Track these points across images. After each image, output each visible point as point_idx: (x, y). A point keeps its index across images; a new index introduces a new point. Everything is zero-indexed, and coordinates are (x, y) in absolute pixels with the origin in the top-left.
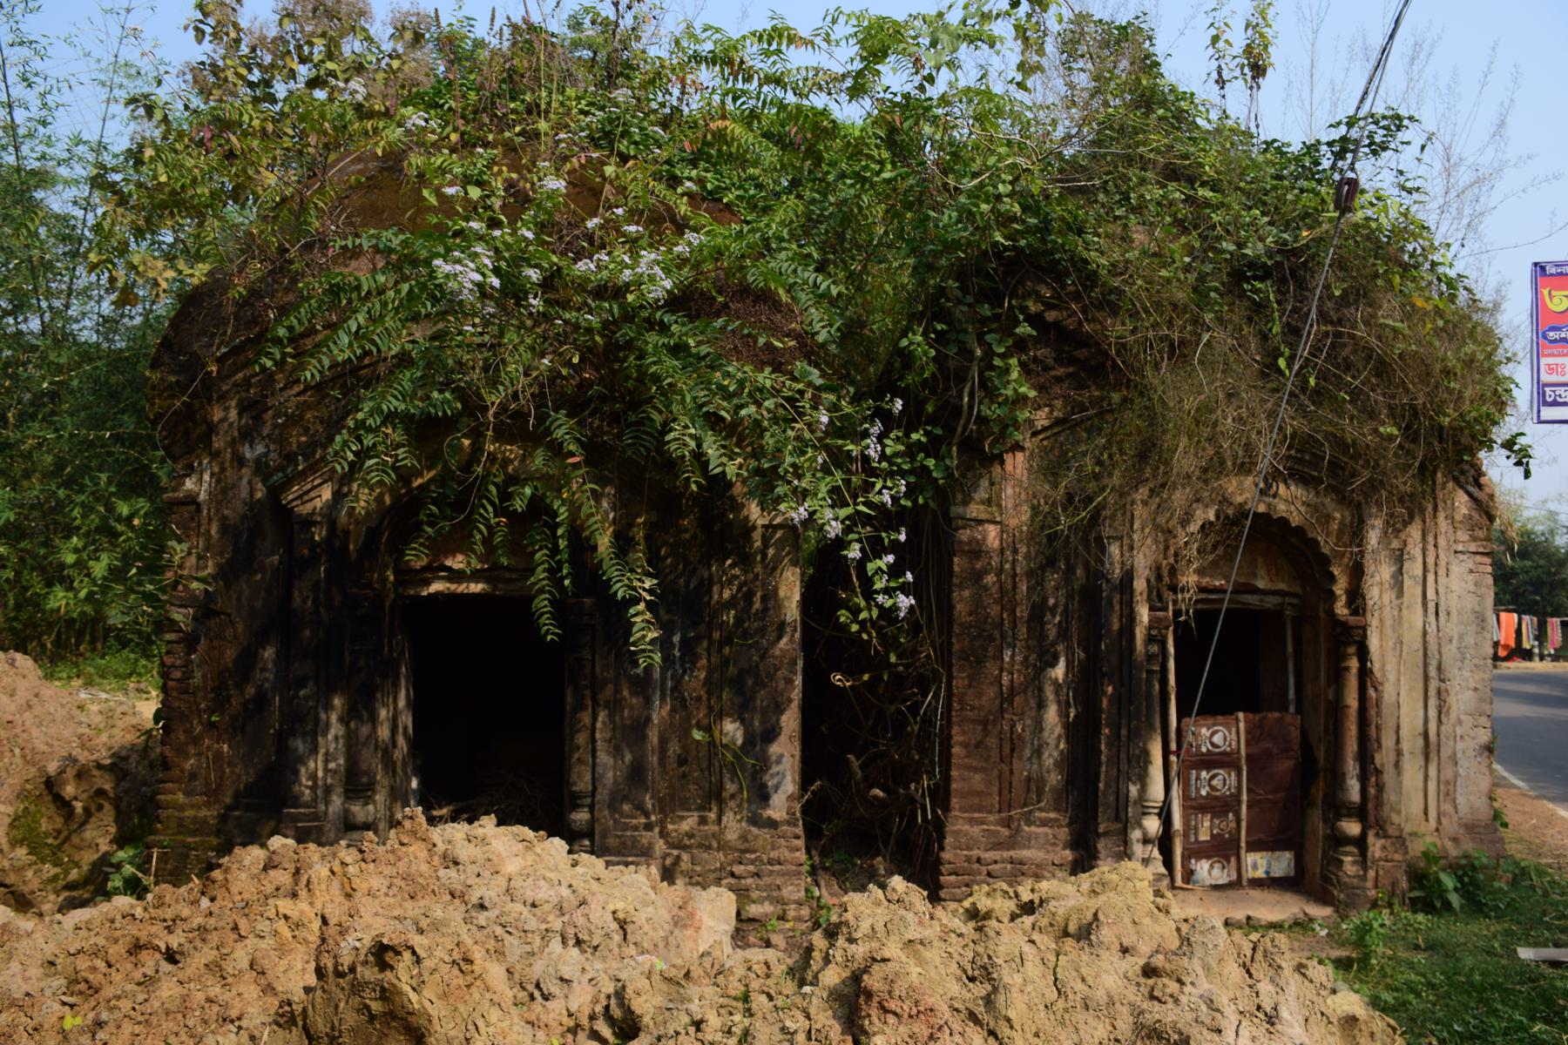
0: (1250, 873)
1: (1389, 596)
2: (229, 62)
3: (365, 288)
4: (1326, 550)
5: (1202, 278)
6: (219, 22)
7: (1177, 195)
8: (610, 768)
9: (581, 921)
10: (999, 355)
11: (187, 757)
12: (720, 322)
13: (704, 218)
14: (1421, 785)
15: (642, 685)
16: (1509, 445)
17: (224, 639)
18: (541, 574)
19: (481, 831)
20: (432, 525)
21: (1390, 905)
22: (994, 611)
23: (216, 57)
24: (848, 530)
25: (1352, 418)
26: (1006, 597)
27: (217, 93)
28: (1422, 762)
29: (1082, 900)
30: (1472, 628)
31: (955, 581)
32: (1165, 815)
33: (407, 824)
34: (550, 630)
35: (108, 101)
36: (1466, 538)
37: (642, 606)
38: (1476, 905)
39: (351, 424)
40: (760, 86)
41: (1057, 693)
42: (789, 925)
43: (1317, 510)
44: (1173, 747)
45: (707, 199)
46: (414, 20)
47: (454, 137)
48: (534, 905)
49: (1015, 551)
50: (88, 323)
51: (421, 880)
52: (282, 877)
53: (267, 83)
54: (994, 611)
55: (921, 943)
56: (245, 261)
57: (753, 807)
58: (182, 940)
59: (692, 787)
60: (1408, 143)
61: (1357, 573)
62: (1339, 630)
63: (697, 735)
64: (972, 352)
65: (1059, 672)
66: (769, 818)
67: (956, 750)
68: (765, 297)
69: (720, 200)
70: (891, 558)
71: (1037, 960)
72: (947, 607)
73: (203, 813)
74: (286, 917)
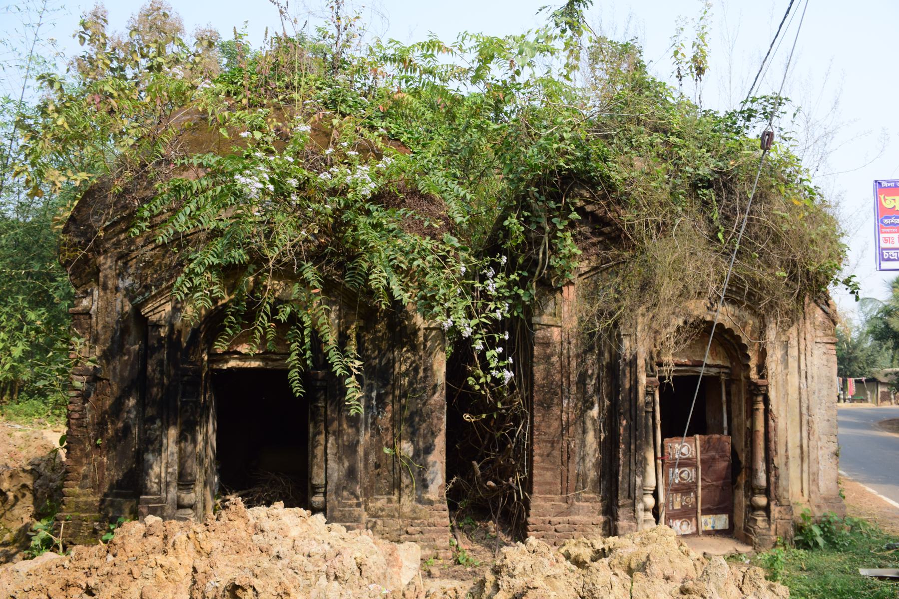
0: (703, 528)
1: (780, 368)
2: (99, 56)
3: (195, 189)
4: (744, 342)
5: (675, 186)
6: (94, 33)
7: (659, 140)
8: (336, 470)
9: (338, 565)
10: (560, 230)
11: (82, 465)
12: (402, 211)
13: (393, 150)
14: (799, 475)
15: (354, 421)
16: (847, 282)
17: (106, 395)
18: (294, 356)
19: (275, 511)
20: (230, 327)
21: (784, 545)
22: (557, 377)
23: (92, 53)
24: (475, 332)
25: (759, 267)
26: (564, 370)
27: (92, 74)
28: (799, 462)
29: (637, 548)
30: (826, 386)
31: (535, 360)
32: (655, 495)
33: (233, 507)
34: (298, 389)
35: (26, 77)
36: (822, 334)
37: (353, 378)
38: (832, 545)
39: (187, 270)
40: (421, 75)
41: (594, 424)
42: (440, 562)
43: (739, 319)
44: (659, 455)
45: (393, 138)
46: (208, 34)
47: (245, 101)
48: (309, 556)
49: (569, 343)
50: (11, 206)
51: (242, 542)
52: (156, 541)
53: (122, 69)
54: (557, 377)
55: (554, 577)
56: (121, 171)
57: (419, 493)
58: (97, 581)
59: (383, 481)
60: (785, 113)
61: (763, 354)
62: (753, 387)
63: (387, 451)
64: (543, 229)
65: (595, 412)
66: (428, 499)
67: (536, 458)
68: (428, 198)
69: (398, 140)
70: (500, 350)
71: (620, 586)
72: (530, 376)
73: (91, 499)
74: (162, 566)
